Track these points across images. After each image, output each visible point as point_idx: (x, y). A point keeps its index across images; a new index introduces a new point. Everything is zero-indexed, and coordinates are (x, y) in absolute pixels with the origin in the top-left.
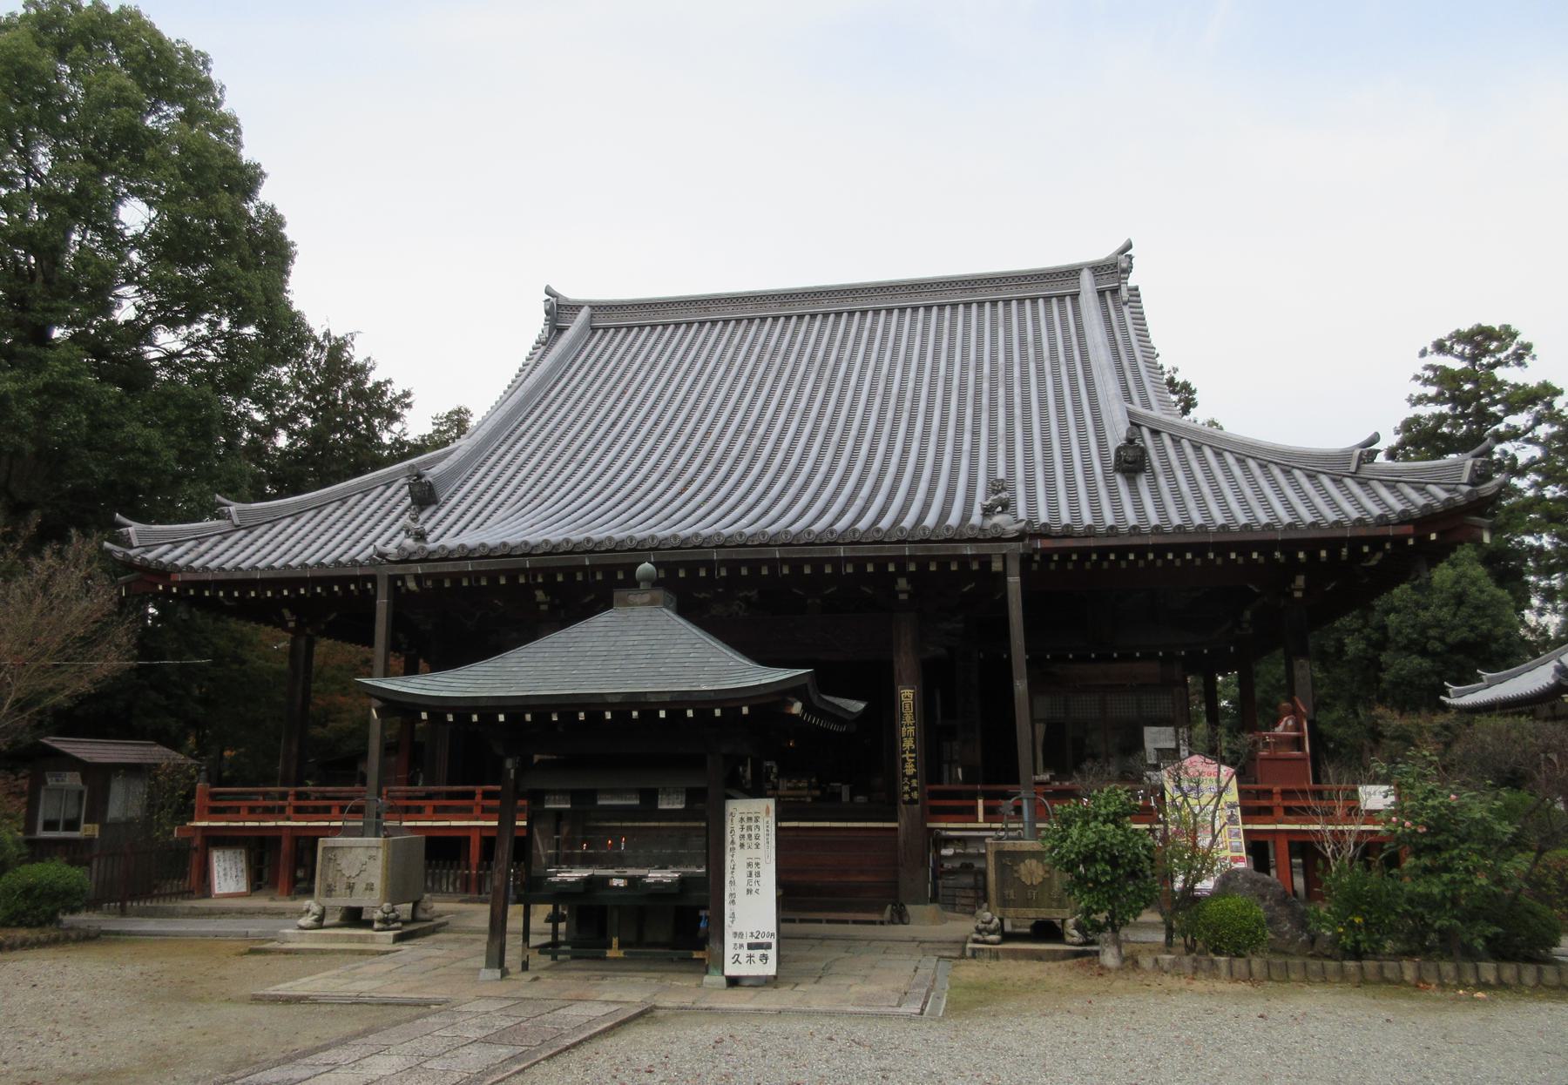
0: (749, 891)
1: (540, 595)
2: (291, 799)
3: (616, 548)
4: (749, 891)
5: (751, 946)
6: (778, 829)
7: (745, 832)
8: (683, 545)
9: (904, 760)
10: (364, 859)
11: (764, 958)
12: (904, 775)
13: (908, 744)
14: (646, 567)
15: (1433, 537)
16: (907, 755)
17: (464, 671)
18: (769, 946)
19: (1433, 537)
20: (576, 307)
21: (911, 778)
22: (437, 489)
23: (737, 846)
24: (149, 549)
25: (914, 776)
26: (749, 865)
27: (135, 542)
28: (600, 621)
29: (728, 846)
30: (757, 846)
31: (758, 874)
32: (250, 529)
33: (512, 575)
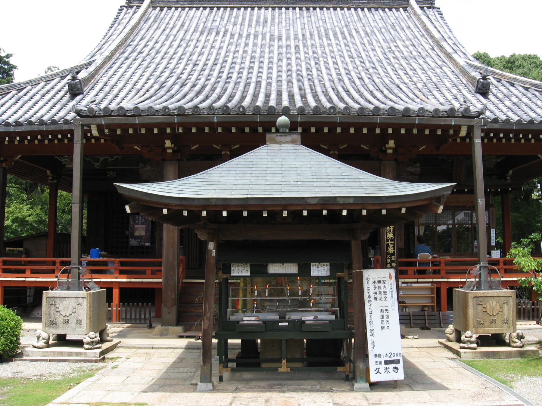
0: (383, 328)
1: (168, 143)
4: (383, 328)
5: (386, 362)
7: (377, 290)
10: (75, 305)
11: (396, 369)
12: (388, 253)
14: (283, 119)
16: (389, 242)
17: (184, 181)
18: (398, 362)
21: (391, 255)
23: (372, 299)
25: (393, 254)
26: (381, 311)
28: (260, 152)
29: (366, 299)
30: (386, 298)
31: (387, 317)
33: (149, 127)
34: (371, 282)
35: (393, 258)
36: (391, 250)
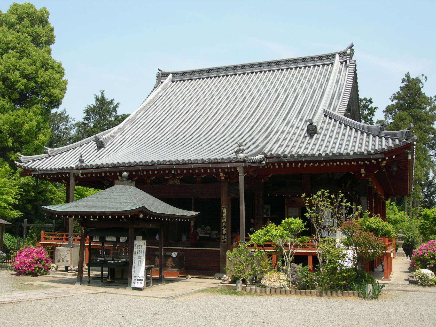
0: (138, 265)
2: (65, 236)
3: (113, 166)
4: (138, 265)
5: (138, 280)
6: (147, 248)
8: (135, 165)
9: (223, 230)
12: (223, 234)
13: (224, 224)
15: (394, 157)
16: (224, 228)
18: (142, 280)
19: (394, 157)
20: (167, 74)
21: (224, 235)
22: (104, 143)
24: (26, 163)
25: (225, 235)
27: (22, 161)
29: (134, 253)
31: (141, 261)
32: (54, 156)
34: (137, 246)
35: (225, 236)
36: (224, 232)
